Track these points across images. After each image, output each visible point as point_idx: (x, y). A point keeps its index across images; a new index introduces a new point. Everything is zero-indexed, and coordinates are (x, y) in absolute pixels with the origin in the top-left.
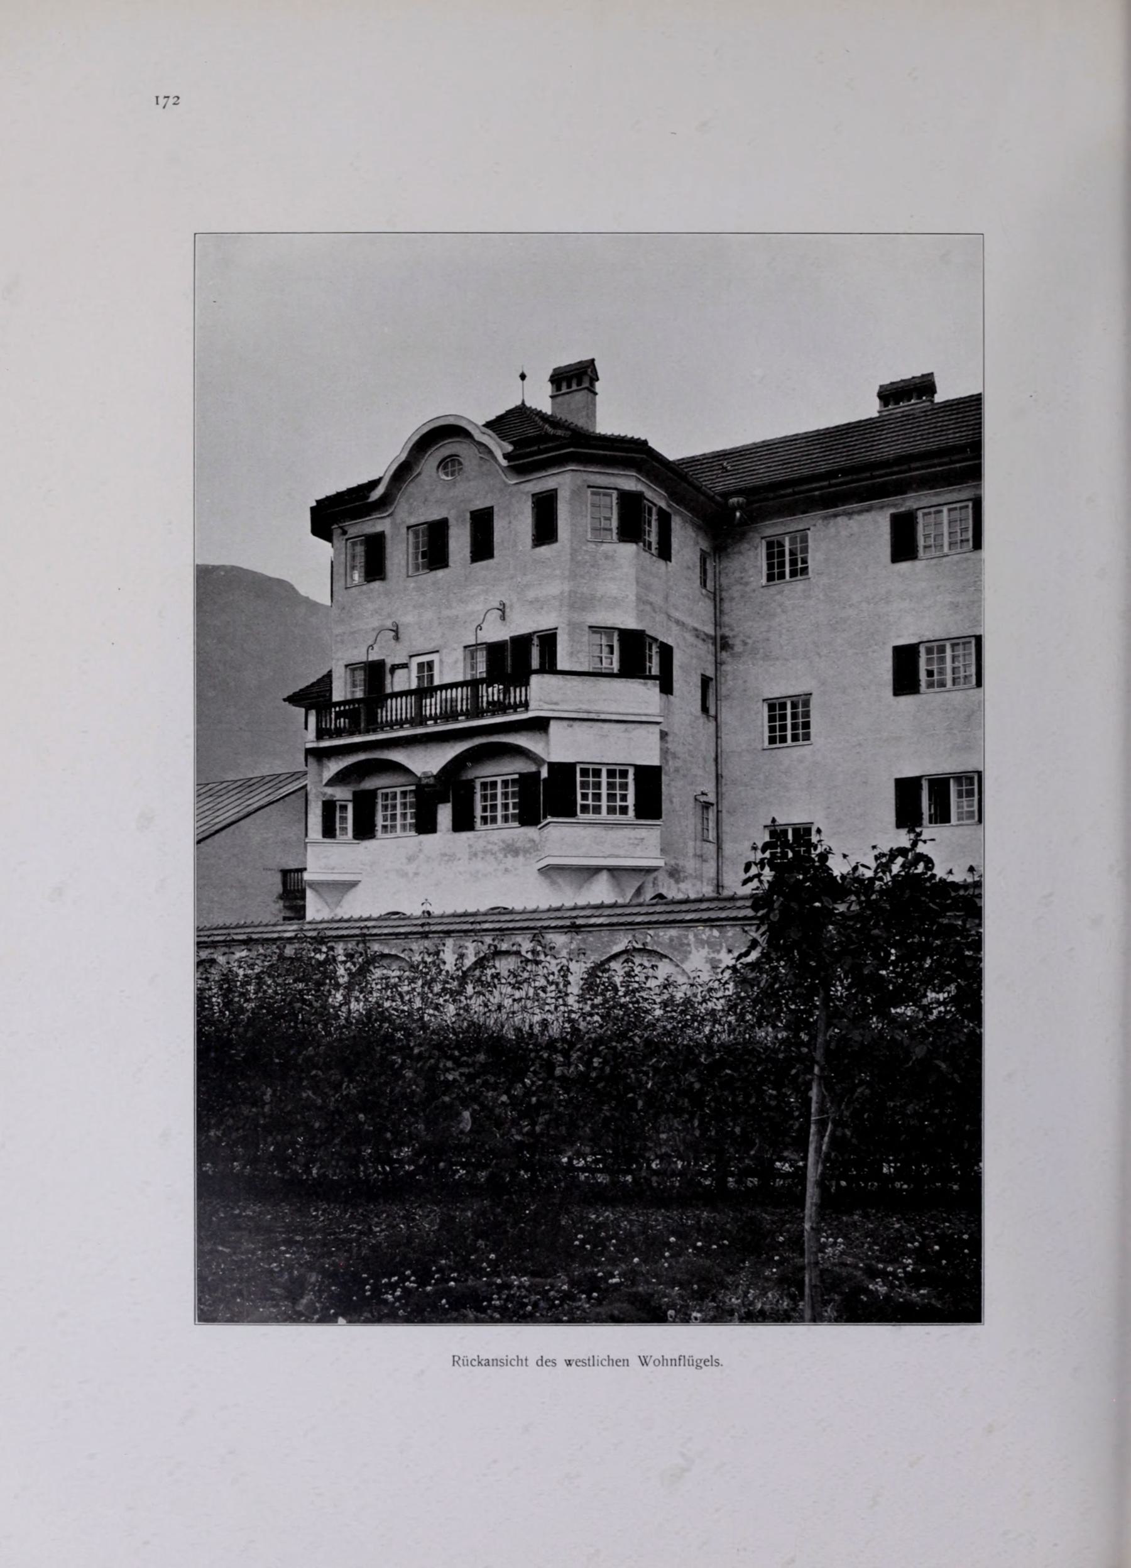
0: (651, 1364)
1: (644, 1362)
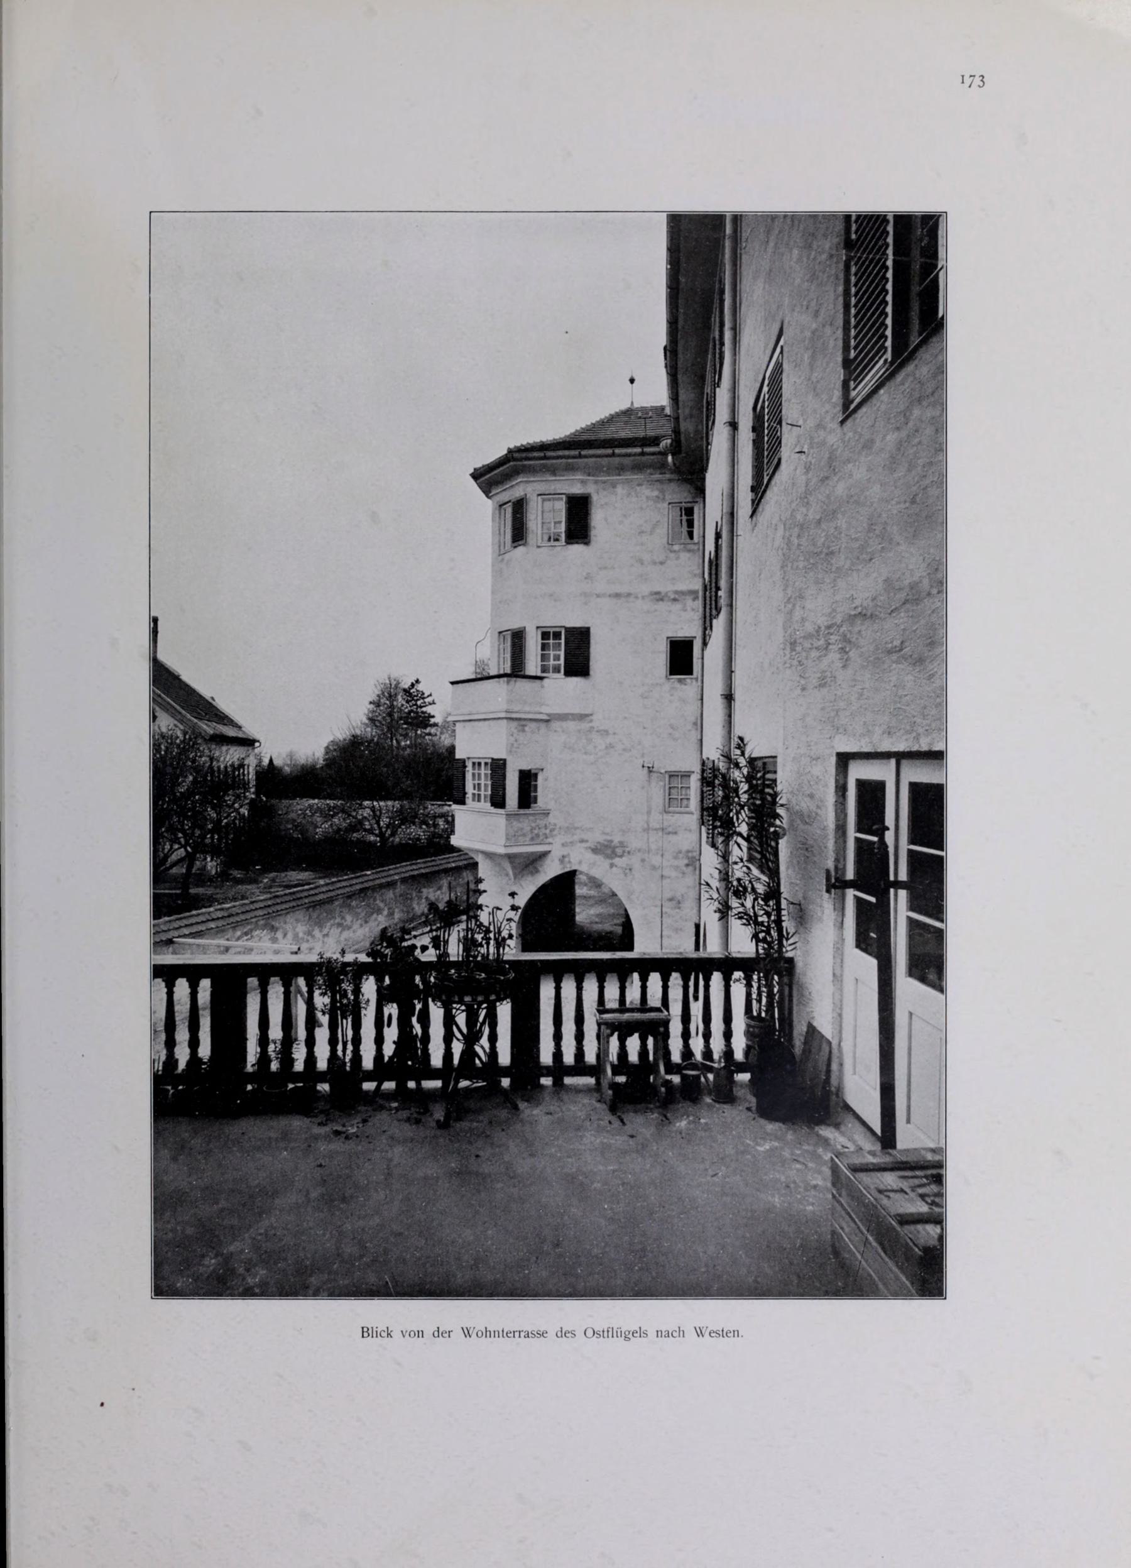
0: (474, 1336)
1: (467, 1333)
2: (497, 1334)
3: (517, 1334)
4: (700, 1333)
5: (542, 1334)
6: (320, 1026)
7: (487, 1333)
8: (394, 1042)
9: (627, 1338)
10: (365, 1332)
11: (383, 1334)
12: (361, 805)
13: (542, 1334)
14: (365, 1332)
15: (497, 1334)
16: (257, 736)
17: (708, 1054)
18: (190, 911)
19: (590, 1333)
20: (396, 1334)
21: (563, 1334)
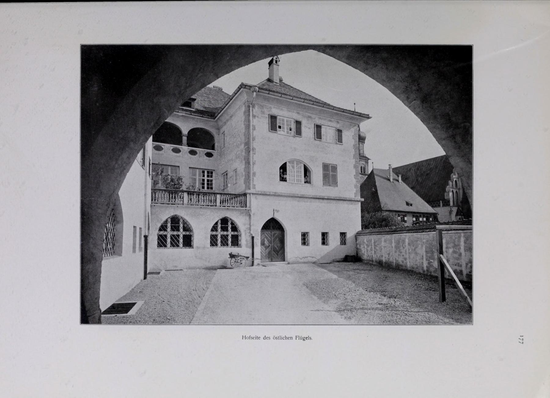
10: (244, 337)
14: (244, 337)
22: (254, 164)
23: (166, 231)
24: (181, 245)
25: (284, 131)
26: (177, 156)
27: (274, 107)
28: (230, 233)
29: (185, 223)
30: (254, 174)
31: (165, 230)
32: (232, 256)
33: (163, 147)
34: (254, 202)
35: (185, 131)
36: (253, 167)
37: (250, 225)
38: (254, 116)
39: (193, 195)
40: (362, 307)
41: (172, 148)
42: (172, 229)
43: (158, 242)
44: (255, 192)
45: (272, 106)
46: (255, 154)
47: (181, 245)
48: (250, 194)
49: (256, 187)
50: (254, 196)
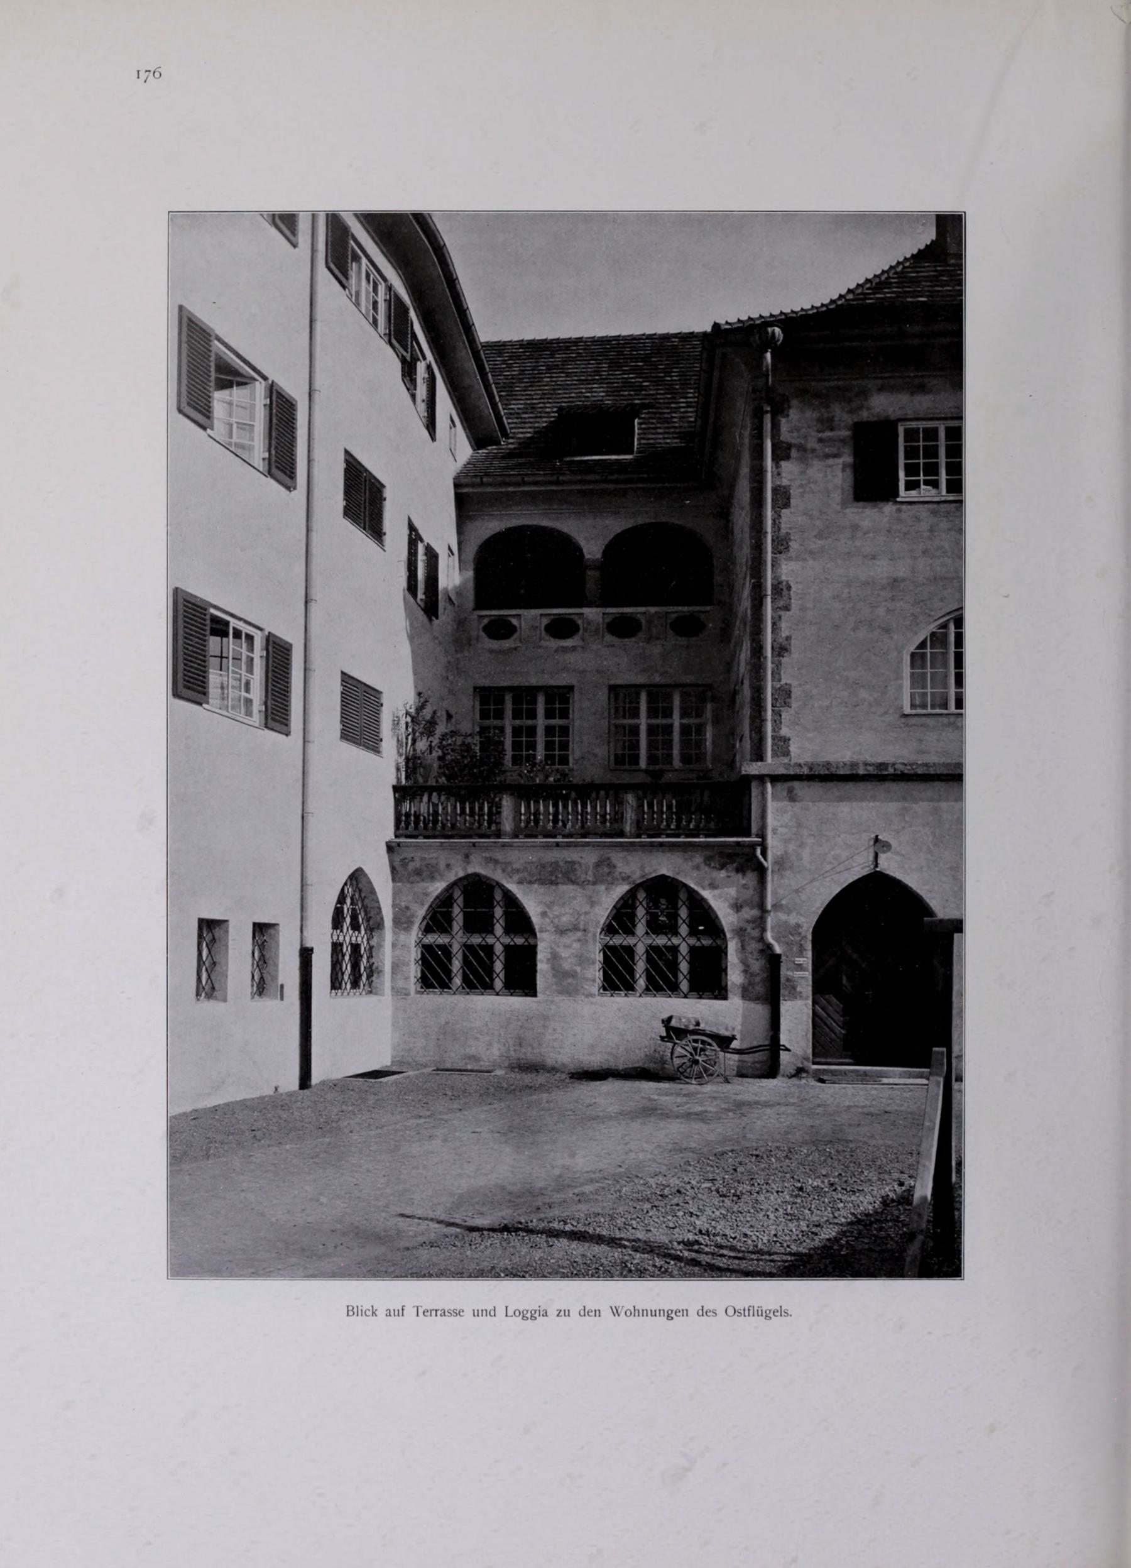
2: (645, 1313)
3: (434, 1313)
4: (616, 1312)
5: (458, 1313)
6: (794, 994)
7: (636, 1312)
8: (716, 326)
9: (670, 1318)
10: (351, 1311)
11: (368, 1313)
12: (811, 769)
13: (458, 1313)
14: (351, 1311)
15: (645, 1313)
16: (899, 183)
17: (575, 804)
18: (826, 1057)
19: (731, 1311)
20: (381, 1313)
21: (703, 1312)
22: (781, 650)
23: (633, 934)
24: (498, 984)
25: (935, 484)
26: (565, 650)
27: (881, 389)
28: (499, 939)
29: (511, 901)
30: (784, 695)
31: (630, 932)
32: (673, 1032)
33: (515, 622)
34: (778, 818)
35: (592, 549)
36: (778, 666)
37: (762, 906)
38: (782, 453)
39: (565, 799)
40: (691, 1237)
41: (545, 621)
42: (654, 927)
43: (605, 975)
44: (782, 771)
45: (871, 384)
46: (787, 608)
47: (498, 984)
48: (761, 778)
49: (793, 748)
50: (782, 787)
